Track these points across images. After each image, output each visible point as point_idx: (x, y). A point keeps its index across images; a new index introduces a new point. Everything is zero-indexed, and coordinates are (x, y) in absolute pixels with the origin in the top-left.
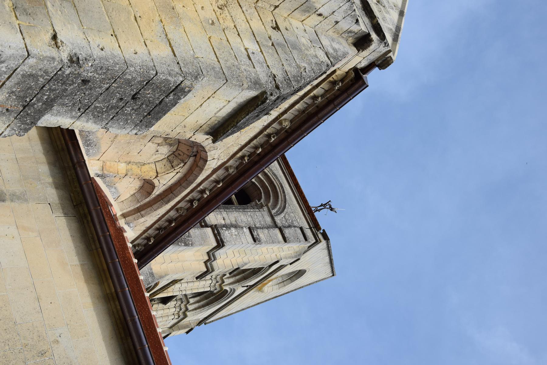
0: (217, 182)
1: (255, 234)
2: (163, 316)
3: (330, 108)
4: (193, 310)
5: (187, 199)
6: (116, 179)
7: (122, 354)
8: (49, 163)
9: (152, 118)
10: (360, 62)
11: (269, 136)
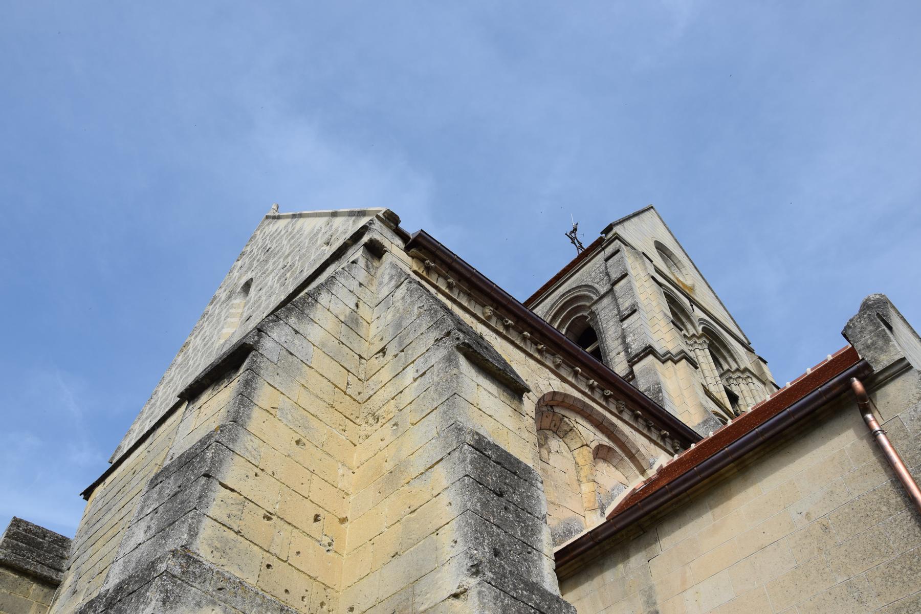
0: (576, 374)
1: (626, 313)
2: (753, 397)
3: (457, 266)
4: (736, 362)
5: (604, 403)
6: (602, 491)
7: (805, 436)
8: (602, 572)
9: (519, 468)
10: (398, 246)
11: (507, 327)
